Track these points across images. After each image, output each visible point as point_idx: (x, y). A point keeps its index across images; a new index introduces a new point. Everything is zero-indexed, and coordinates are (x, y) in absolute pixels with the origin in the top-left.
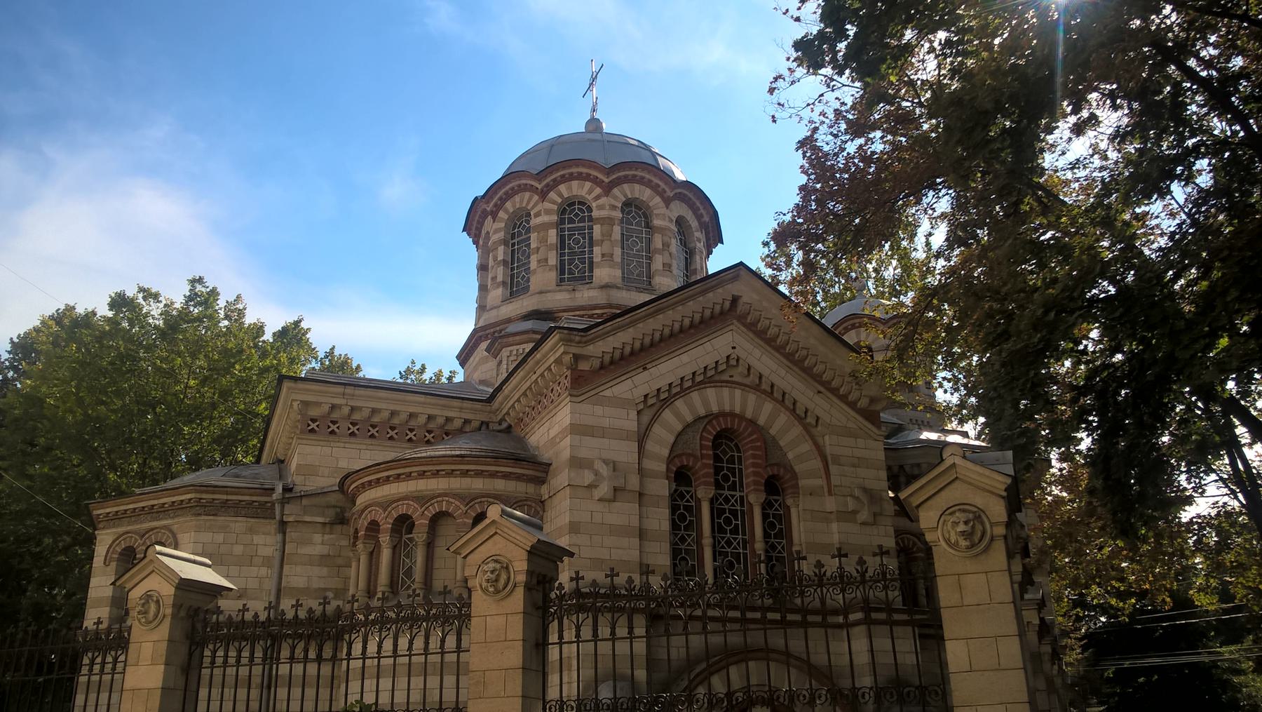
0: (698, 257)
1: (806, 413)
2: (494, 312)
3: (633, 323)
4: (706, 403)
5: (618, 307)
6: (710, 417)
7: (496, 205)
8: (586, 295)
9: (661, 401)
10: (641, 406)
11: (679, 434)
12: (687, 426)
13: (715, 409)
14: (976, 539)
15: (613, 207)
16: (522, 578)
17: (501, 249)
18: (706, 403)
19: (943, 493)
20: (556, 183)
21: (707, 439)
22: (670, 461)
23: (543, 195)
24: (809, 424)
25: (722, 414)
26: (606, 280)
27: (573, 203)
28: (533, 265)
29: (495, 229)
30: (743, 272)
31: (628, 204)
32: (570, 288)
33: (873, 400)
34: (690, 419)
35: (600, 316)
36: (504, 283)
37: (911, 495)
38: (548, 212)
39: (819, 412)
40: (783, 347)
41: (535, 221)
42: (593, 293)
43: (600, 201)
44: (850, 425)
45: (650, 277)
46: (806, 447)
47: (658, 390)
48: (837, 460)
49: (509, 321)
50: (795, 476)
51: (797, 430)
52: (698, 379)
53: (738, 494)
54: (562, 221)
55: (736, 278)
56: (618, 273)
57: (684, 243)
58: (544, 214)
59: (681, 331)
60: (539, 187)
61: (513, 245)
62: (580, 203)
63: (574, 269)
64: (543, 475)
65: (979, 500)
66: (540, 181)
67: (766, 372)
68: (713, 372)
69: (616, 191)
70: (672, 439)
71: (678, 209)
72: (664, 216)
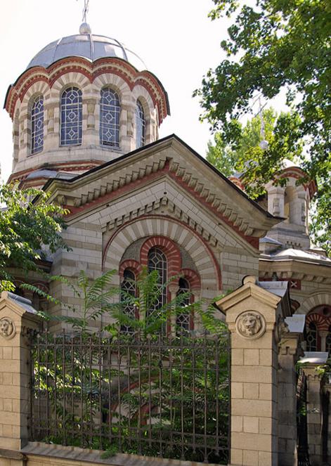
0: (151, 127)
1: (209, 237)
2: (22, 164)
3: (100, 177)
4: (145, 229)
5: (97, 162)
6: (148, 238)
7: (22, 91)
8: (76, 154)
9: (119, 226)
10: (105, 230)
11: (128, 248)
12: (133, 243)
13: (151, 233)
14: (255, 328)
15: (96, 91)
16: (19, 330)
17: (26, 121)
18: (145, 229)
19: (241, 303)
20: (59, 74)
21: (145, 252)
22: (121, 264)
23: (51, 83)
24: (211, 244)
25: (156, 237)
26: (90, 143)
27: (70, 89)
28: (45, 133)
29: (22, 107)
30: (174, 141)
31: (105, 89)
32: (67, 149)
33: (255, 230)
34: (135, 238)
35: (85, 168)
36: (28, 144)
37: (223, 303)
38: (54, 95)
39: (220, 239)
40: (198, 193)
41: (46, 102)
42: (82, 152)
43: (87, 87)
44: (238, 246)
45: (118, 140)
46: (208, 259)
47: (116, 220)
48: (227, 268)
49: (31, 170)
50: (199, 277)
51: (202, 248)
52: (141, 213)
53: (162, 286)
54: (63, 102)
55: (170, 145)
56: (98, 138)
57: (142, 117)
58: (51, 96)
59: (132, 181)
60: (49, 77)
61: (33, 118)
62: (75, 88)
63: (69, 137)
64: (48, 268)
65: (262, 310)
66: (49, 73)
67: (185, 210)
68: (151, 209)
69: (97, 79)
70: (123, 251)
71: (140, 91)
72: (130, 97)
